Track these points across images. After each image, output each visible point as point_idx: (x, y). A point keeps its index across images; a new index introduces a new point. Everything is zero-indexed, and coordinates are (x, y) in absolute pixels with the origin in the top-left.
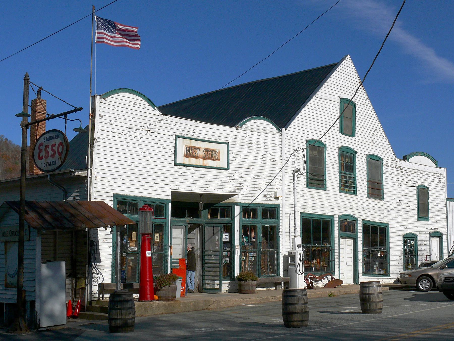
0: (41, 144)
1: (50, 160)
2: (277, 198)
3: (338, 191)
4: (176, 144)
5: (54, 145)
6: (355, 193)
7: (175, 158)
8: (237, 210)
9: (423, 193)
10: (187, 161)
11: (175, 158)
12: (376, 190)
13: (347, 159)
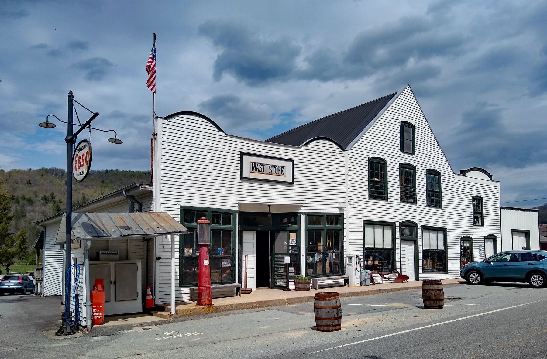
4: (241, 161)
6: (415, 203)
7: (241, 173)
8: (303, 217)
9: (478, 201)
10: (253, 176)
11: (241, 173)
12: (435, 199)
13: (407, 173)
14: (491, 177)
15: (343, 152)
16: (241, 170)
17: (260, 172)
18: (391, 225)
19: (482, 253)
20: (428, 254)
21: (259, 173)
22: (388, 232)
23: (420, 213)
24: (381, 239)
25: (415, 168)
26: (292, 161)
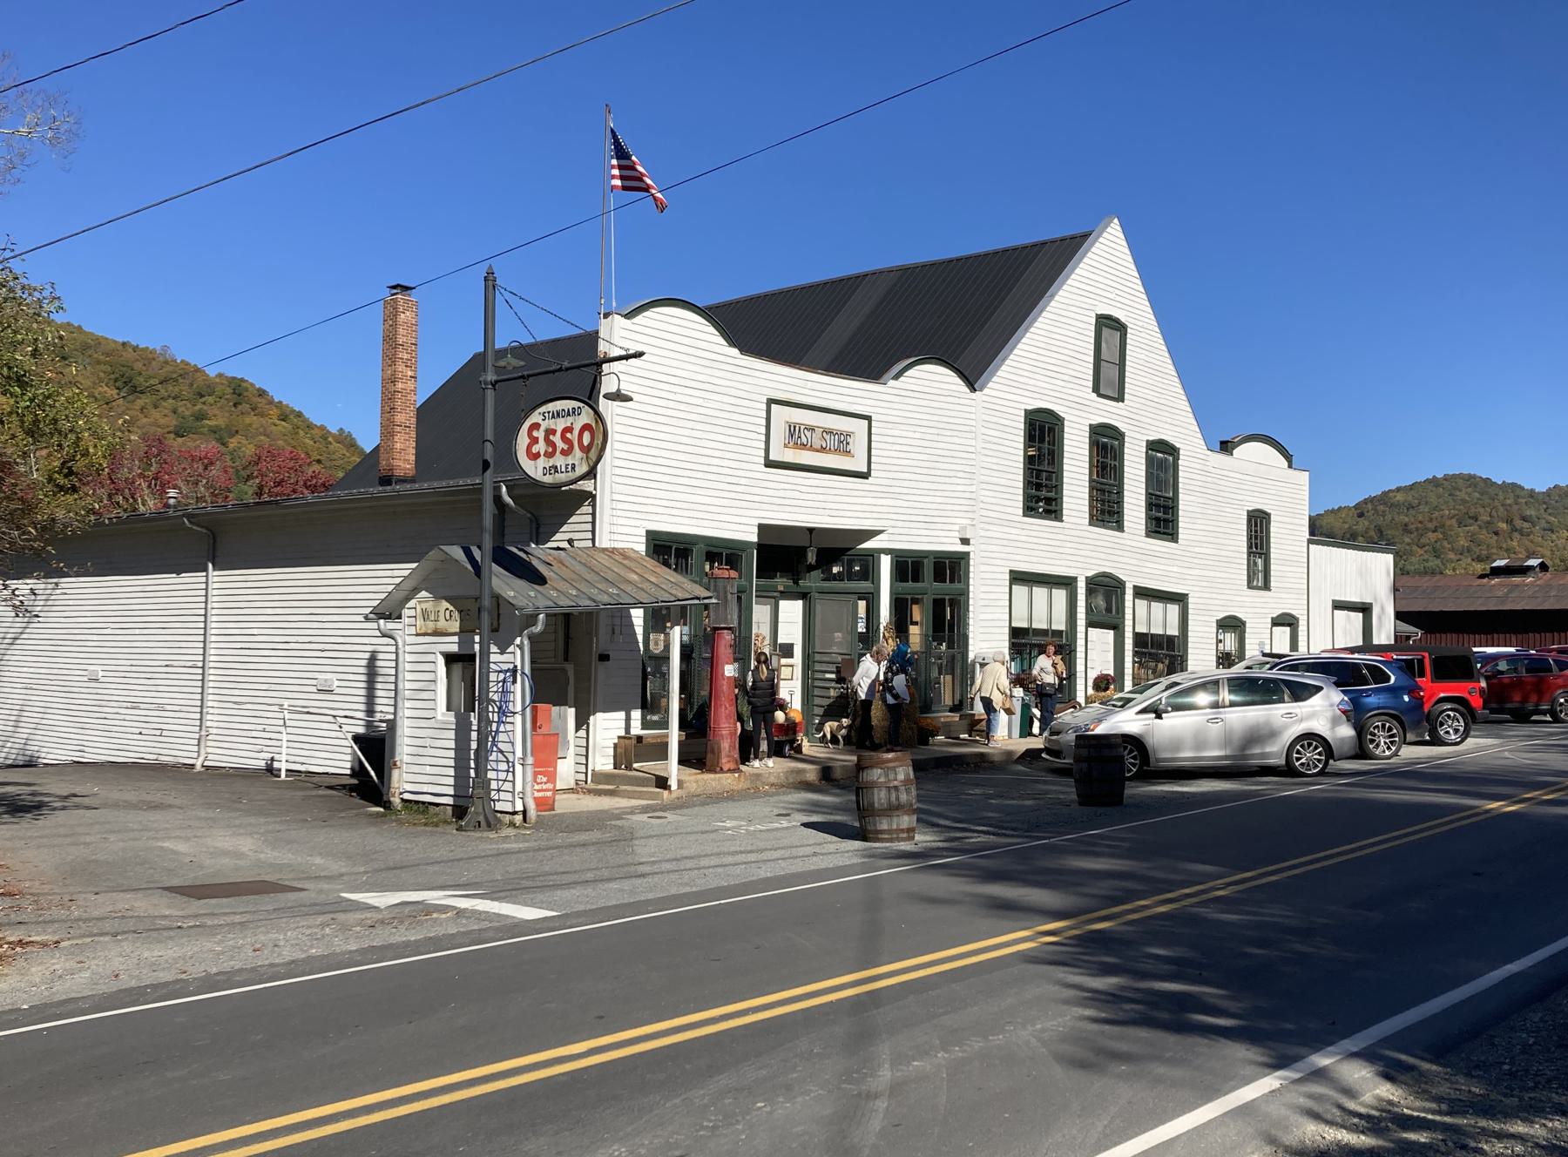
0: (536, 426)
1: (559, 461)
2: (965, 541)
3: (1021, 512)
5: (569, 429)
7: (767, 450)
8: (886, 563)
9: (1258, 524)
10: (790, 456)
11: (767, 450)
12: (1163, 521)
13: (1106, 446)
14: (1288, 457)
15: (973, 395)
16: (767, 442)
17: (803, 446)
18: (1068, 583)
19: (1262, 640)
20: (1143, 642)
21: (804, 449)
22: (1060, 595)
23: (1130, 554)
24: (1047, 610)
25: (1122, 435)
26: (868, 418)
